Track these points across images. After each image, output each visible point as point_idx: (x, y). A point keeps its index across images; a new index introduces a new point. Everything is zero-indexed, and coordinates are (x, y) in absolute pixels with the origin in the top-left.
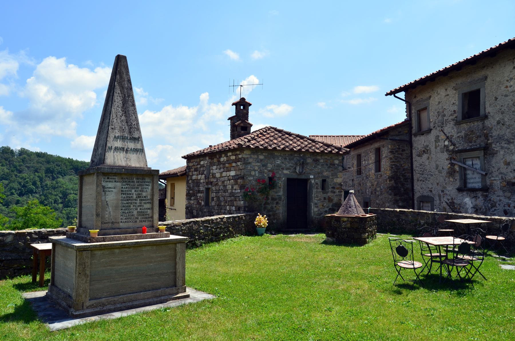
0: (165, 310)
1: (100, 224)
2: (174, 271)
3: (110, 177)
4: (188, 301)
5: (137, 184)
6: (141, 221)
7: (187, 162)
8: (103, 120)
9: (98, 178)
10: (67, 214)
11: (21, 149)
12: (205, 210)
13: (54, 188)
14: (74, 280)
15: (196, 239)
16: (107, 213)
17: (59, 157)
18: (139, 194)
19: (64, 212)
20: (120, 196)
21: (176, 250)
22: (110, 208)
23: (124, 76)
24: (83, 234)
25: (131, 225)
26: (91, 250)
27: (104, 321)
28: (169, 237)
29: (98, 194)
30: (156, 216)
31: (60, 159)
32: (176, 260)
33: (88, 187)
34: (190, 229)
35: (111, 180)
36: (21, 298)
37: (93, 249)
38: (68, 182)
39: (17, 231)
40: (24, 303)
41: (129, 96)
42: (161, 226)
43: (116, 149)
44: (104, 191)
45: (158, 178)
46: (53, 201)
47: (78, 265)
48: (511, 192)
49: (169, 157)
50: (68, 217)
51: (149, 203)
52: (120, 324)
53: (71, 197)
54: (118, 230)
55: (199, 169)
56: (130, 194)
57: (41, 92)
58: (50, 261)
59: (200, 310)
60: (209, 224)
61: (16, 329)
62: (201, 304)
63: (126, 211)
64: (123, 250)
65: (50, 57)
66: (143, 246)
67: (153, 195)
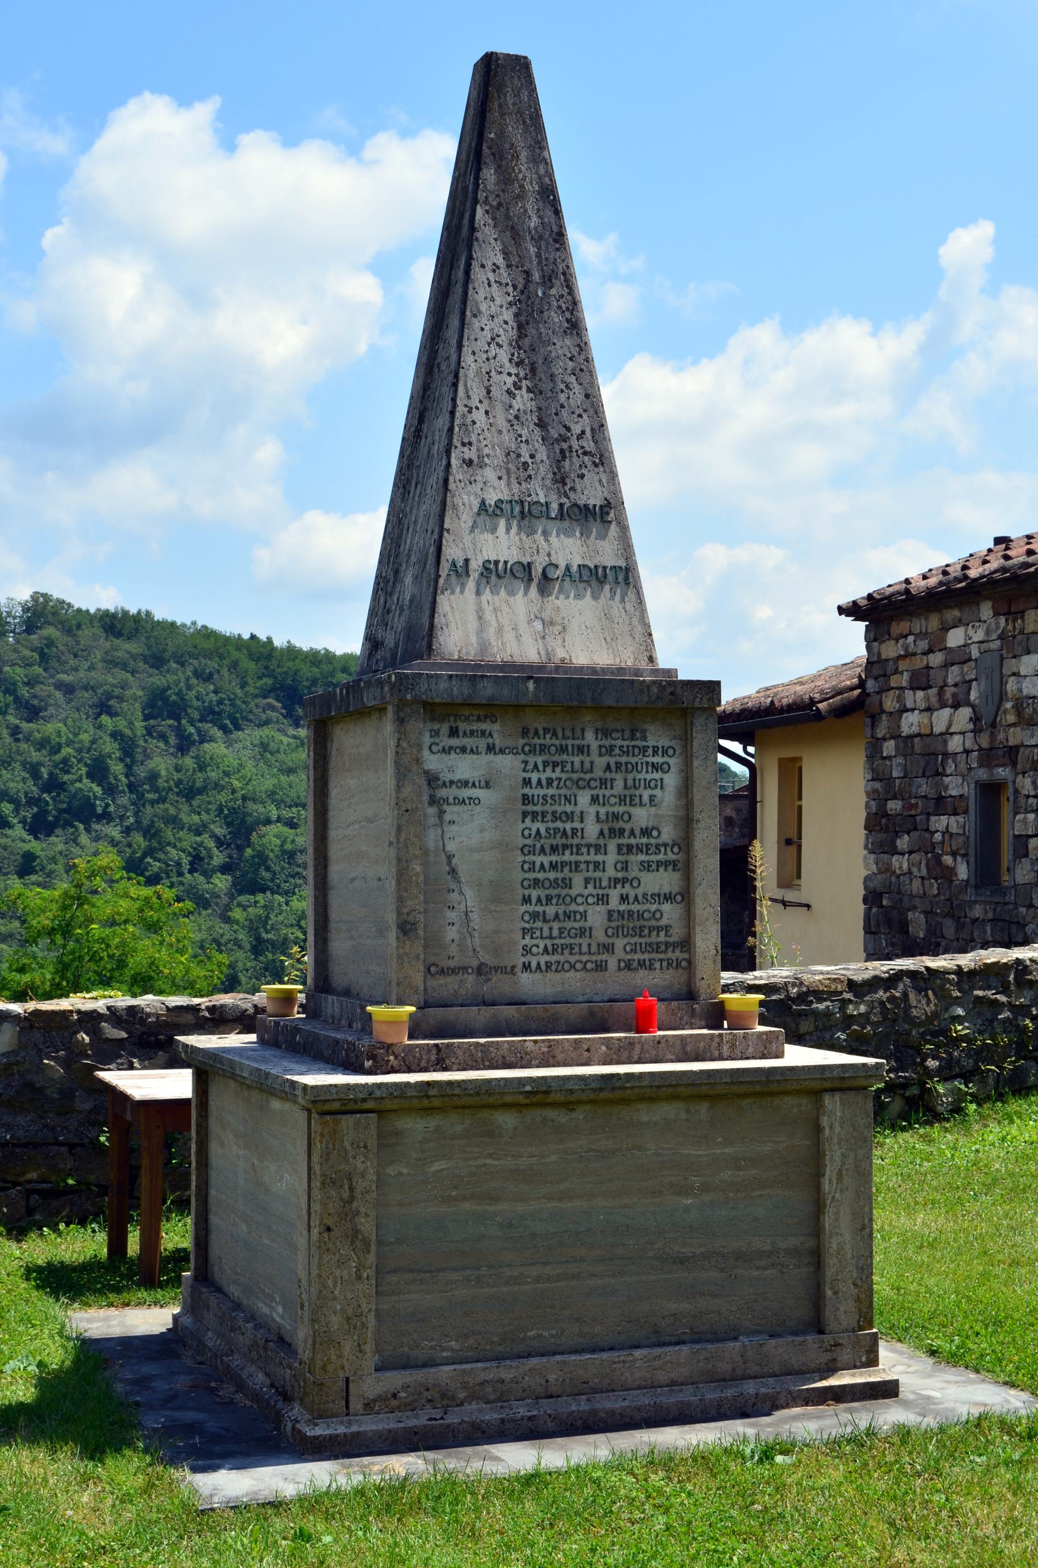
0: (767, 1455)
1: (418, 978)
2: (810, 1243)
3: (463, 726)
4: (889, 1416)
5: (601, 762)
6: (628, 966)
7: (872, 639)
8: (421, 420)
9: (401, 734)
10: (255, 927)
11: (35, 596)
12: (977, 912)
13: (189, 793)
14: (301, 1257)
15: (929, 1074)
16: (452, 916)
17: (207, 633)
18: (616, 817)
19: (237, 914)
20: (516, 830)
21: (818, 1129)
22: (469, 893)
23: (523, 168)
24: (337, 1029)
25: (573, 981)
26: (380, 1113)
27: (451, 1480)
28: (780, 1055)
29: (406, 814)
30: (708, 939)
31: (210, 645)
32: (818, 1187)
33: (352, 783)
34: (895, 1014)
35: (468, 742)
36: (60, 1333)
37: (387, 1104)
38: (256, 760)
39: (32, 1006)
40: (77, 1362)
41: (548, 280)
42: (738, 993)
43: (494, 573)
44: (433, 801)
45: (714, 725)
46: (185, 861)
47: (316, 1184)
48: (197, 904)
49: (764, 612)
50: (259, 939)
51: (666, 864)
52: (530, 1506)
53: (272, 837)
54: (510, 1011)
55: (937, 677)
56: (569, 817)
57: (117, 297)
58: (186, 1158)
59: (959, 1472)
60: (1005, 990)
61: (45, 1480)
62: (963, 1440)
63: (551, 910)
64: (538, 1114)
65: (147, 95)
66: (641, 1099)
67: (687, 822)
